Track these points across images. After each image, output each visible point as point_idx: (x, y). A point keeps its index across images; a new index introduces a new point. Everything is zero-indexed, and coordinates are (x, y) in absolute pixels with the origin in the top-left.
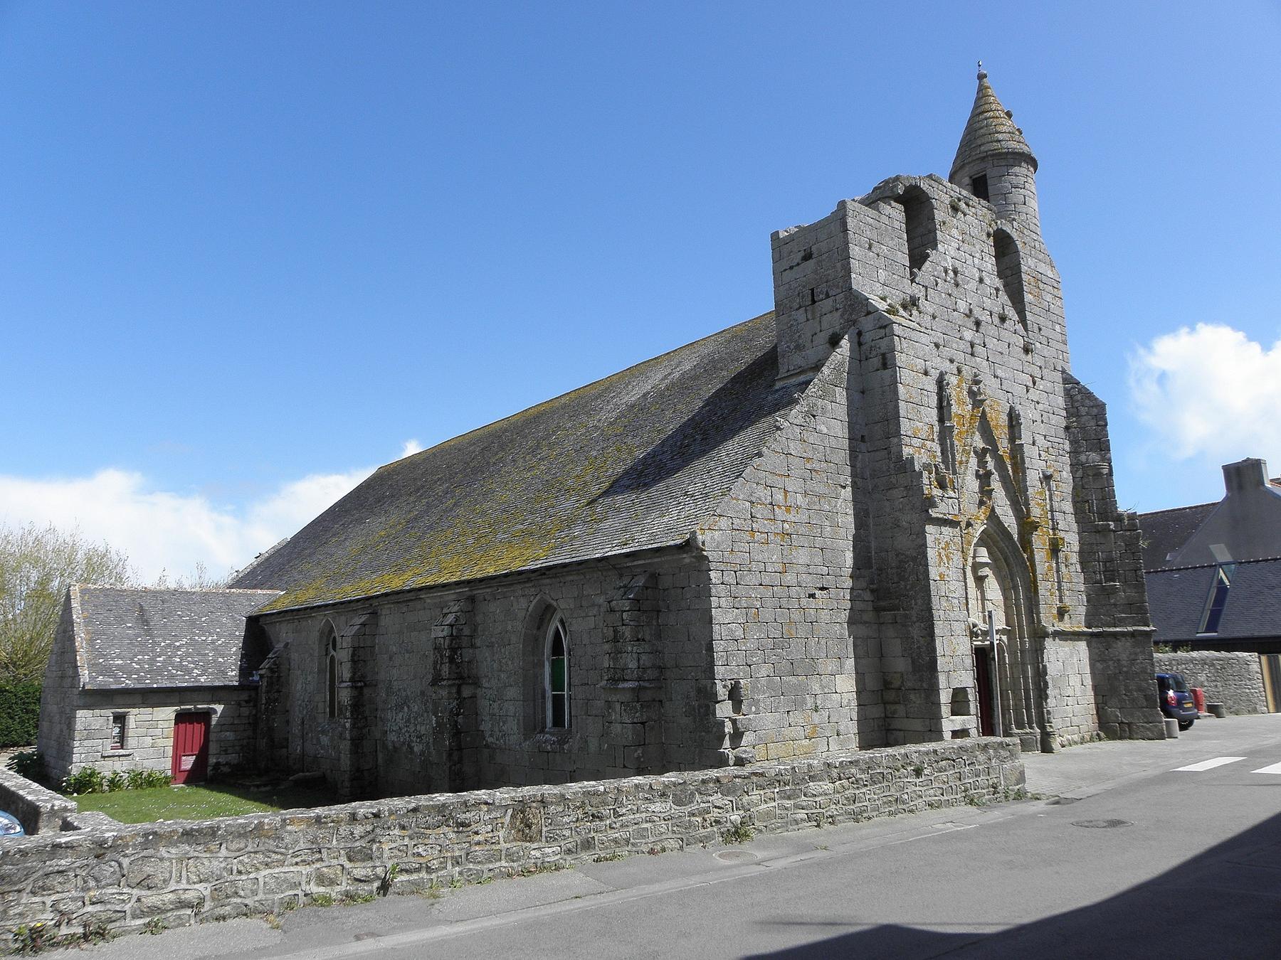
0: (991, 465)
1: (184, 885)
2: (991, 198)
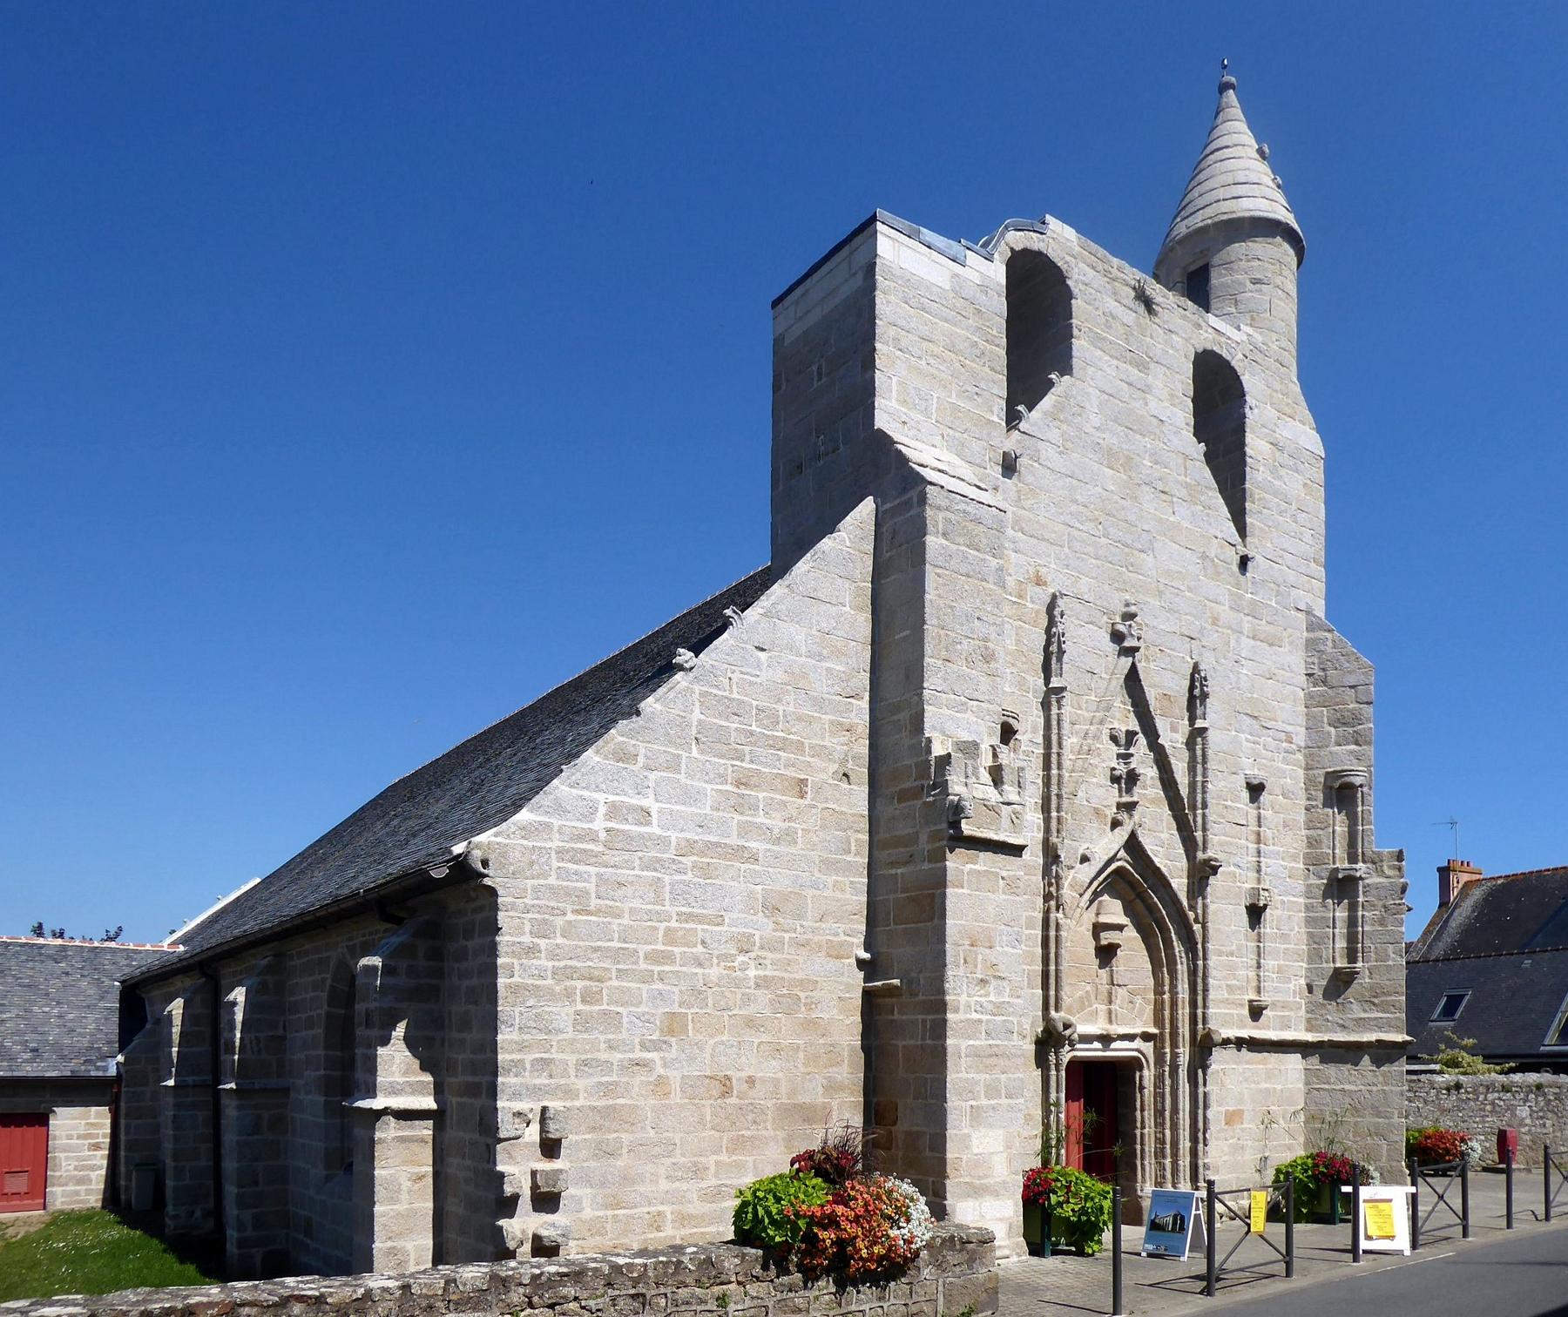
2: (1214, 303)
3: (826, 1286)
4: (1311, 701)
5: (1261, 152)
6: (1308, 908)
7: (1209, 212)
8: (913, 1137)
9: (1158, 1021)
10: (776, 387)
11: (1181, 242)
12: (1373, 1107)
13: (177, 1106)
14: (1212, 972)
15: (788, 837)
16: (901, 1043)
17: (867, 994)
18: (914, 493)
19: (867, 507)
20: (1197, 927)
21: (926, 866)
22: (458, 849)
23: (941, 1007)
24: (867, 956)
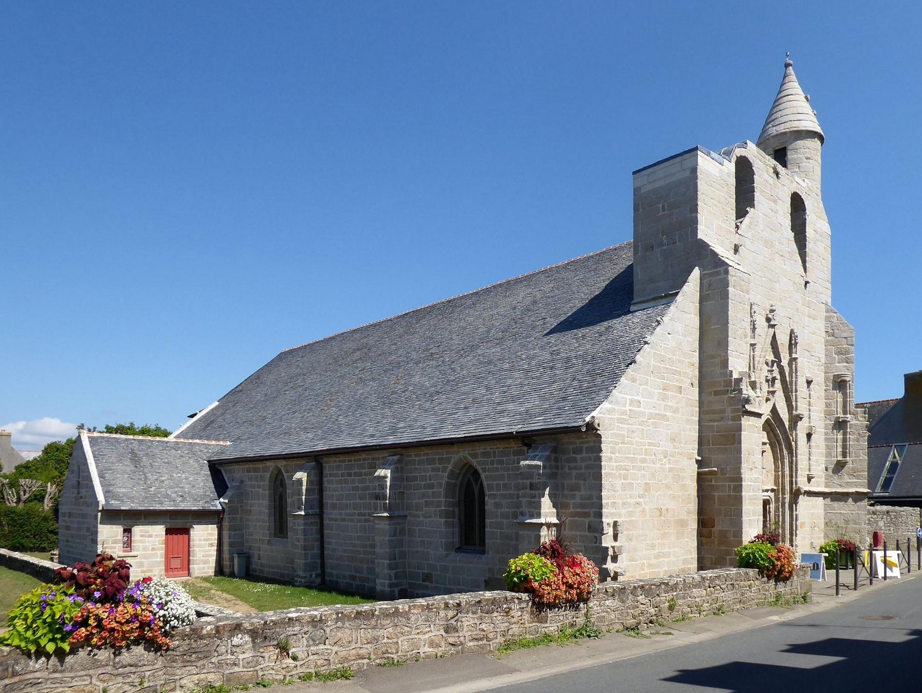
0: (776, 373)
1: (359, 645)
2: (789, 166)
3: (772, 582)
4: (827, 343)
5: (806, 98)
6: (826, 434)
7: (788, 125)
8: (723, 534)
9: (776, 483)
10: (636, 209)
11: (773, 137)
12: (853, 520)
13: (305, 524)
14: (799, 463)
15: (676, 411)
16: (716, 494)
17: (699, 474)
18: (722, 269)
19: (696, 273)
20: (793, 443)
21: (730, 422)
22: (588, 419)
23: (740, 479)
24: (700, 458)
